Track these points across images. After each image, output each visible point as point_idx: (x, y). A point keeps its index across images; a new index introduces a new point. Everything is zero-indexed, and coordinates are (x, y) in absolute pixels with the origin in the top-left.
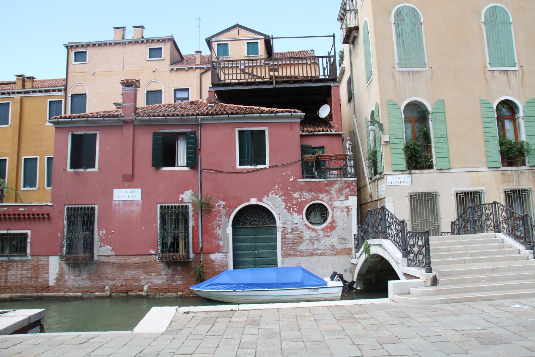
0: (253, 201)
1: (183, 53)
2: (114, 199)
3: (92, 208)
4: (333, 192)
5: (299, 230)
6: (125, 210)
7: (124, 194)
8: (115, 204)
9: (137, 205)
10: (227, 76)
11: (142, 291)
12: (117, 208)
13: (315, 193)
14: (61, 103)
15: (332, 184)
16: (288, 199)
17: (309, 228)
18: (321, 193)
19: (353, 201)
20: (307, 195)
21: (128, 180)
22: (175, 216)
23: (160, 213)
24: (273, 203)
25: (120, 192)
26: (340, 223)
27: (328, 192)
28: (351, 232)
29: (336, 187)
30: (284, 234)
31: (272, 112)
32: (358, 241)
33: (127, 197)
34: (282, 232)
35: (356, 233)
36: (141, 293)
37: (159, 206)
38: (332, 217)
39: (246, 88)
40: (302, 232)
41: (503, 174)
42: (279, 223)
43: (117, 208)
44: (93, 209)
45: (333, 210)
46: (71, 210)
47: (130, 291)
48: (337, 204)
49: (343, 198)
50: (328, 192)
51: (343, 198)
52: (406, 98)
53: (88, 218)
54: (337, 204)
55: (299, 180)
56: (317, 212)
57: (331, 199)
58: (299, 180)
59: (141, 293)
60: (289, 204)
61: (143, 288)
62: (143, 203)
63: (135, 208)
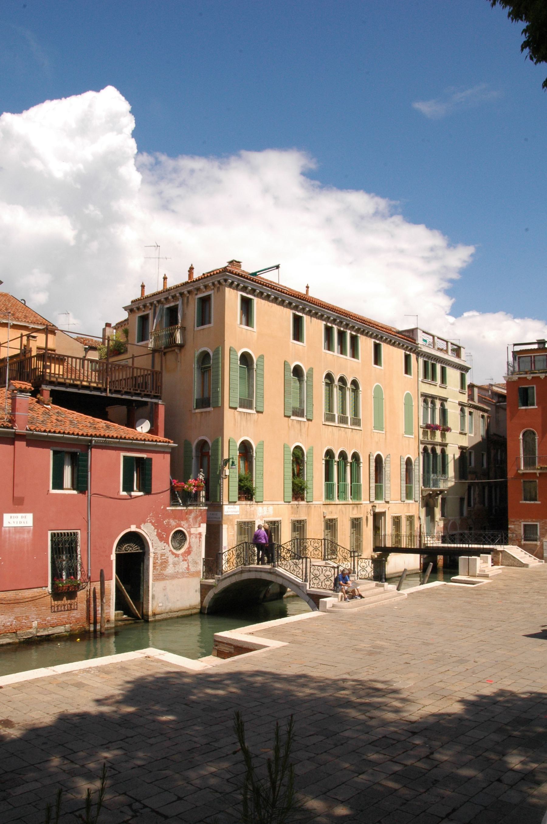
0: (133, 528)
1: (82, 357)
2: (4, 525)
3: (74, 533)
4: (191, 520)
5: (166, 555)
6: (15, 539)
7: (15, 520)
8: (5, 531)
9: (29, 532)
10: (69, 375)
11: (31, 628)
12: (7, 536)
13: (179, 521)
14: (537, 527)
15: (191, 511)
16: (158, 525)
17: (173, 553)
18: (182, 520)
19: (203, 529)
20: (173, 523)
21: (18, 504)
22: (69, 544)
23: (52, 540)
24: (148, 531)
25: (11, 517)
26: (194, 549)
27: (187, 519)
28: (201, 556)
29: (193, 515)
30: (155, 558)
31: (166, 442)
32: (278, 552)
33: (18, 522)
34: (154, 557)
35: (204, 557)
36: (31, 630)
37: (49, 533)
38: (190, 543)
39: (81, 391)
40: (168, 557)
41: (292, 507)
42: (152, 550)
43: (7, 536)
44: (75, 534)
45: (190, 536)
46: (65, 535)
47: (19, 629)
48: (193, 530)
49: (197, 525)
50: (187, 519)
51: (197, 525)
52: (241, 437)
53: (62, 545)
54: (193, 530)
55: (168, 508)
56: (180, 537)
57: (189, 527)
58: (168, 508)
59: (31, 630)
60: (160, 531)
61: (32, 625)
62: (34, 529)
63: (26, 536)
